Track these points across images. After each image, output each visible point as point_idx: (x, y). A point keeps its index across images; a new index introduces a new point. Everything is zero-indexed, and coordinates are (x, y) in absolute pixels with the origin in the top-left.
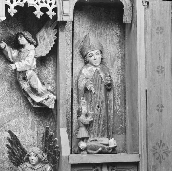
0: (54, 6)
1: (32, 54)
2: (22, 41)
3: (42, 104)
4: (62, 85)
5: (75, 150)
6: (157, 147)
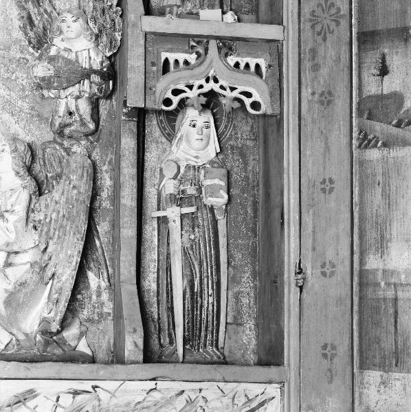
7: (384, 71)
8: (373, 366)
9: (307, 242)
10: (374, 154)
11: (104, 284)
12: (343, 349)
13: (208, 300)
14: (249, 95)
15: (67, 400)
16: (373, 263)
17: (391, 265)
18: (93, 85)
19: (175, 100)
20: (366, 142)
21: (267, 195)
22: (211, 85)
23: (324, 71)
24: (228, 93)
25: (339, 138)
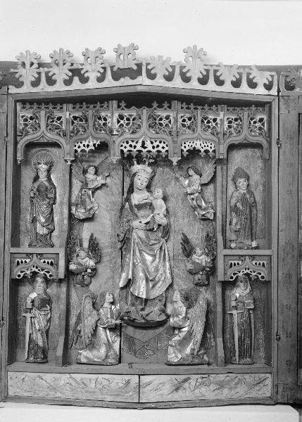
0: (213, 148)
1: (198, 181)
11: (212, 336)
13: (247, 341)
15: (200, 380)
18: (240, 362)
19: (234, 277)
21: (268, 304)
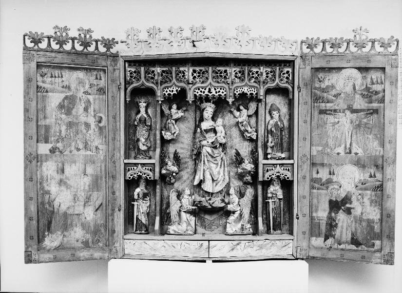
1: (246, 114)
2: (241, 108)
3: (251, 138)
4: (259, 129)
5: (266, 158)
6: (306, 161)
7: (318, 173)
8: (314, 236)
9: (299, 209)
10: (315, 191)
12: (307, 232)
14: (286, 176)
16: (314, 214)
17: (319, 215)
19: (270, 178)
20: (313, 188)
22: (278, 174)
23: (304, 171)
24: (282, 176)
25: (307, 187)
